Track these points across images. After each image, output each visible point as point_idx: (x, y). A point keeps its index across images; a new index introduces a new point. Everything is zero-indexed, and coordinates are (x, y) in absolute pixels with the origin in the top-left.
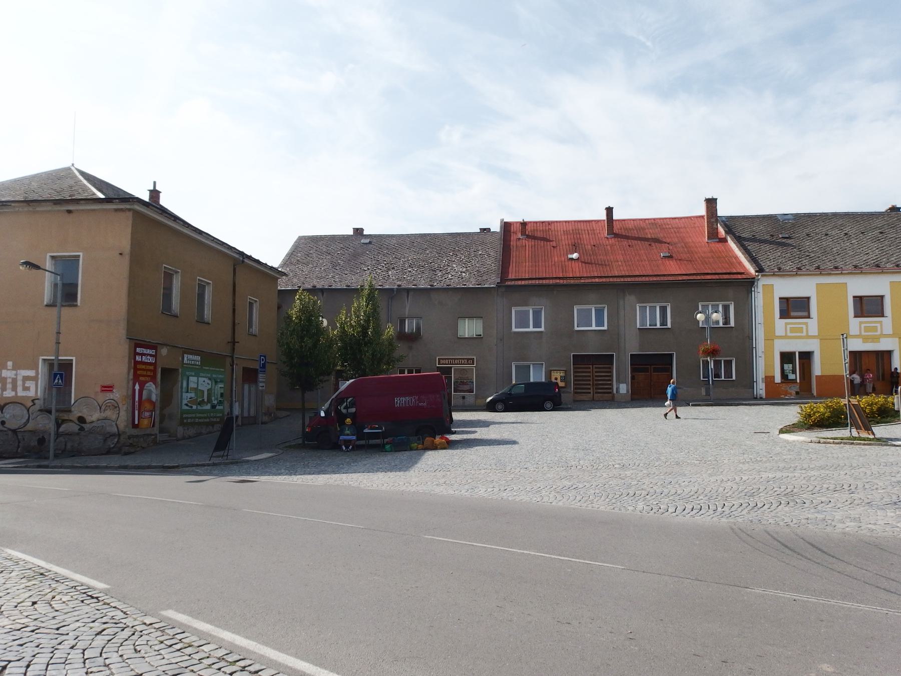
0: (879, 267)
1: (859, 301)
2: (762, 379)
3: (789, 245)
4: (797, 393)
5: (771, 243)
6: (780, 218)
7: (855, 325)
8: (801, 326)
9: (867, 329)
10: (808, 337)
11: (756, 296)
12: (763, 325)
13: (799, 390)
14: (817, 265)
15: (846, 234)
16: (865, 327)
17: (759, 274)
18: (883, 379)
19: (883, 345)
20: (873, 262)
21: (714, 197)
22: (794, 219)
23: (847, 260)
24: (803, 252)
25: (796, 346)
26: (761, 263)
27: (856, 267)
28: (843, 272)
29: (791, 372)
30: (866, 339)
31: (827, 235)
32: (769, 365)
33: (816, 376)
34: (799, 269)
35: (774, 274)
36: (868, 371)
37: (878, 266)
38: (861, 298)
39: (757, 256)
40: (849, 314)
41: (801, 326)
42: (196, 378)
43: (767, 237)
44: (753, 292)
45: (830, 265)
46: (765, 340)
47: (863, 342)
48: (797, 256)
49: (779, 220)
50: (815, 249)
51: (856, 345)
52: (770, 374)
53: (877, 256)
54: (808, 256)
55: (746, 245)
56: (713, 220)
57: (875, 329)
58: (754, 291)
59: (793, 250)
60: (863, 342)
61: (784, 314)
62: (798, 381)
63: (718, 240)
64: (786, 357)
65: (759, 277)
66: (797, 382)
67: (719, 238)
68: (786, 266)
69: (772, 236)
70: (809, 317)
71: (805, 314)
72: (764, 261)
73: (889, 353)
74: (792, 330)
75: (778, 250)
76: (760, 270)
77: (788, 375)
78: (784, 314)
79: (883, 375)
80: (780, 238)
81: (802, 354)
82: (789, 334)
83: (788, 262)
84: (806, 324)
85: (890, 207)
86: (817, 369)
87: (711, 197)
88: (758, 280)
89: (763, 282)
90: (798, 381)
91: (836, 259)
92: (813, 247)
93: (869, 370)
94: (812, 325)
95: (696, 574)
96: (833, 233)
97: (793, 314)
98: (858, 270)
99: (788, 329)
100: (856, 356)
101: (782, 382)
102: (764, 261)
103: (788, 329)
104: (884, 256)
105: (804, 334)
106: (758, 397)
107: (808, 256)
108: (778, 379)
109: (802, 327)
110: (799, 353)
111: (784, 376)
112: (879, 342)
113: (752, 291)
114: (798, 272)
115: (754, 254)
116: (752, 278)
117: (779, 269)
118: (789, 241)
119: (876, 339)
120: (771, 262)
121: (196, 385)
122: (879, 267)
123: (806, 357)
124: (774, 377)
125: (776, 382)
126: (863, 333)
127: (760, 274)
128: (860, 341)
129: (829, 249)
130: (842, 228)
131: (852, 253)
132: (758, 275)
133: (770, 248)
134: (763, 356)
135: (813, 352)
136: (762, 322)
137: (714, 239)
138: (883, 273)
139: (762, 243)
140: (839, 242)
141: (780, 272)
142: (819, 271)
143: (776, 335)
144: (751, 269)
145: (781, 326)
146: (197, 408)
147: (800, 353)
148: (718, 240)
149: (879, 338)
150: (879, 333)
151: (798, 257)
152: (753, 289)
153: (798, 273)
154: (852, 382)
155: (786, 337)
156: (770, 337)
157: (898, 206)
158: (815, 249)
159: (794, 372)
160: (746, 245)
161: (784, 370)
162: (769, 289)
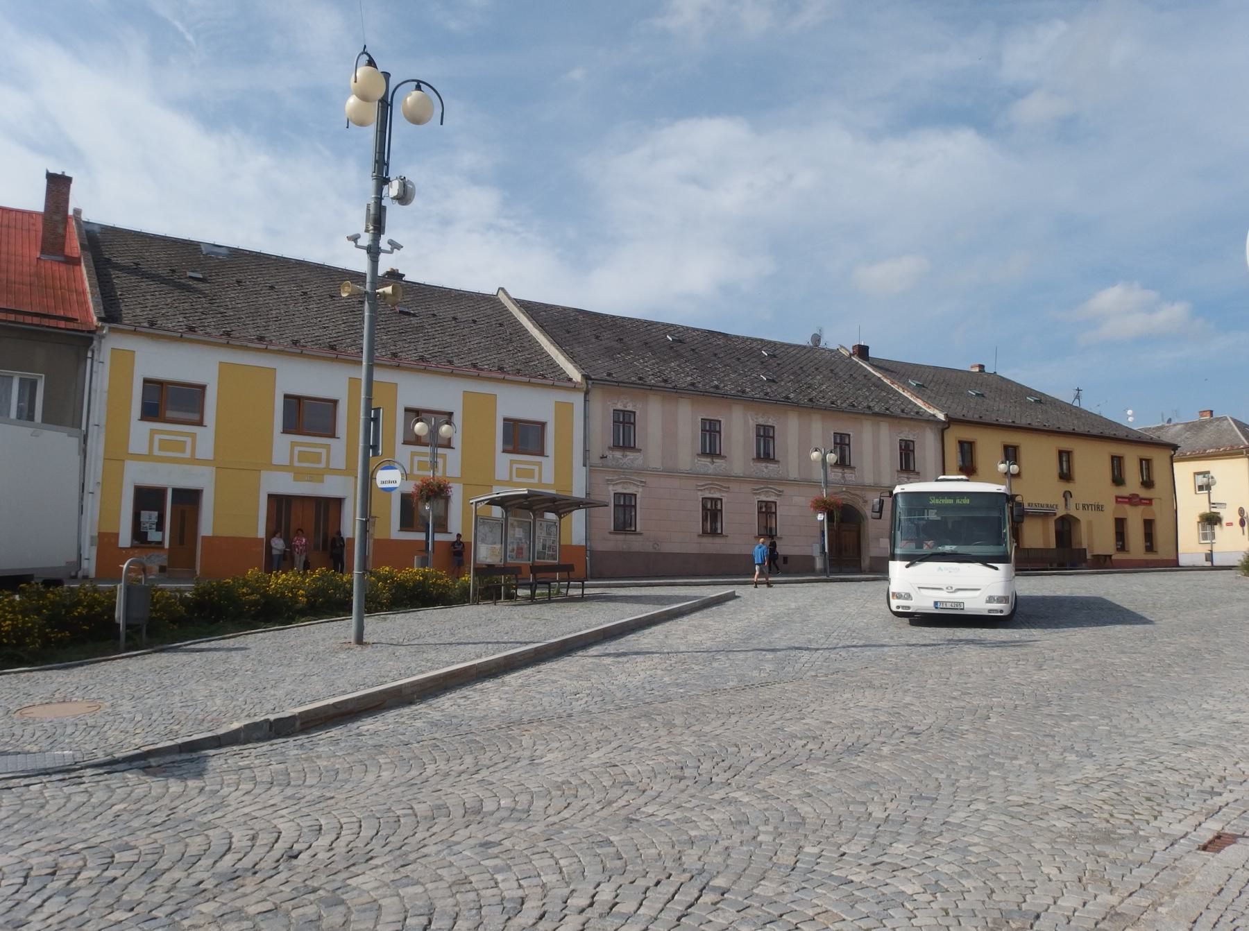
0: (335, 350)
1: (295, 404)
2: (92, 537)
3: (201, 292)
4: (162, 569)
5: (163, 280)
6: (203, 249)
7: (283, 445)
8: (532, 467)
9: (303, 457)
10: (194, 461)
11: (94, 369)
12: (104, 429)
13: (165, 564)
14: (228, 329)
15: (305, 293)
16: (419, 461)
17: (104, 324)
18: (325, 548)
19: (328, 488)
20: (329, 340)
21: (67, 174)
22: (228, 256)
23: (287, 332)
24: (216, 305)
25: (169, 477)
26: (123, 308)
27: (295, 343)
28: (269, 347)
29: (154, 526)
30: (299, 475)
31: (272, 288)
32: (109, 510)
33: (203, 537)
34: (191, 329)
35: (135, 330)
36: (300, 532)
37: (333, 348)
38: (299, 399)
39: (122, 297)
40: (275, 427)
41: (532, 467)
42: (210, 456)
43: (163, 271)
44: (89, 361)
45: (254, 333)
46: (104, 459)
47: (295, 480)
48: (201, 310)
49: (201, 251)
50: (239, 306)
51: (287, 485)
52: (108, 529)
53: (339, 334)
54: (221, 313)
55: (113, 276)
56: (58, 218)
57: (181, 447)
58: (92, 358)
59: (198, 300)
60: (295, 480)
61: (151, 412)
62: (167, 545)
63: (62, 259)
64: (147, 498)
65: (104, 332)
66: (163, 548)
67: (66, 256)
68: (169, 322)
69: (173, 271)
70: (200, 423)
71: (196, 417)
72: (132, 307)
73: (339, 502)
74: (521, 473)
75: (171, 295)
76: (111, 316)
77: (147, 533)
78: (151, 412)
79: (325, 541)
80: (186, 278)
81: (179, 494)
82: (156, 452)
83: (178, 316)
84: (193, 436)
85: (389, 270)
86: (206, 527)
87: (60, 173)
88: (103, 337)
89: (111, 345)
90: (167, 545)
91: (268, 326)
92: (239, 301)
93: (302, 531)
94: (204, 439)
95: (539, 547)
96: (286, 288)
97: (170, 414)
98: (298, 349)
99: (296, 453)
100: (280, 504)
101: (133, 547)
102: (132, 307)
103: (296, 453)
104: (350, 336)
105: (187, 455)
106: (80, 574)
107: (221, 313)
108: (125, 539)
109: (185, 442)
110: (175, 490)
111: (139, 534)
112: (322, 481)
113: (87, 358)
114: (189, 334)
115: (119, 293)
116: (89, 332)
117: (152, 324)
118: (201, 286)
119: (317, 476)
120: (143, 311)
121: (145, 451)
122: (335, 350)
123: (189, 499)
124: (117, 535)
125: (120, 545)
126: (296, 464)
127: (107, 326)
128: (288, 477)
129: (265, 310)
130: (304, 284)
131: (301, 323)
132: (102, 328)
133: (158, 289)
134: (98, 492)
135: (202, 490)
136: (103, 422)
137: (53, 254)
138: (337, 359)
139: (147, 278)
140: (287, 303)
141: (153, 330)
142: (228, 340)
143: (130, 452)
144: (93, 314)
145: (141, 433)
146: (843, 477)
147: (175, 490)
148: (62, 259)
149: (323, 475)
150: (323, 465)
151: (202, 313)
152: (89, 354)
153: (185, 335)
154: (269, 548)
155: (149, 457)
156: (117, 455)
157: (400, 272)
158: (239, 306)
159: (160, 526)
160: (113, 276)
161: (140, 523)
162: (124, 361)
